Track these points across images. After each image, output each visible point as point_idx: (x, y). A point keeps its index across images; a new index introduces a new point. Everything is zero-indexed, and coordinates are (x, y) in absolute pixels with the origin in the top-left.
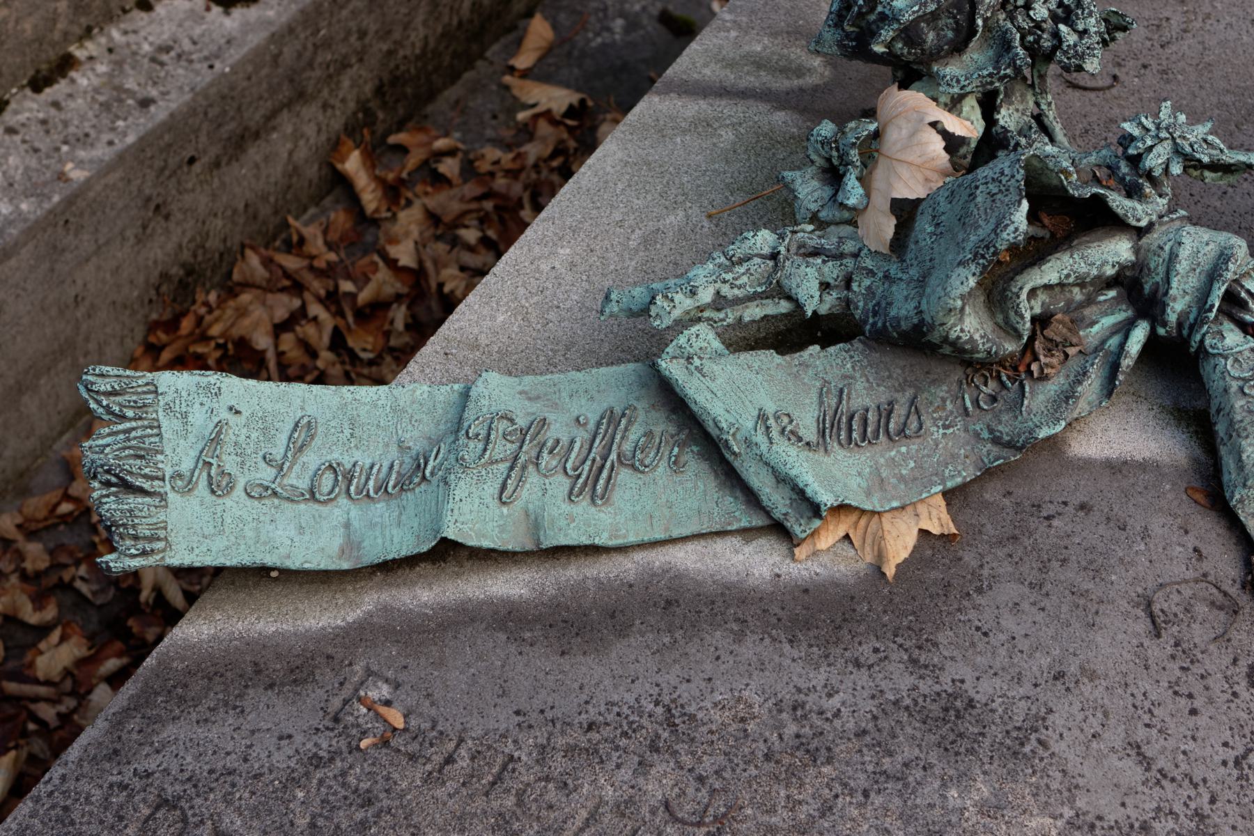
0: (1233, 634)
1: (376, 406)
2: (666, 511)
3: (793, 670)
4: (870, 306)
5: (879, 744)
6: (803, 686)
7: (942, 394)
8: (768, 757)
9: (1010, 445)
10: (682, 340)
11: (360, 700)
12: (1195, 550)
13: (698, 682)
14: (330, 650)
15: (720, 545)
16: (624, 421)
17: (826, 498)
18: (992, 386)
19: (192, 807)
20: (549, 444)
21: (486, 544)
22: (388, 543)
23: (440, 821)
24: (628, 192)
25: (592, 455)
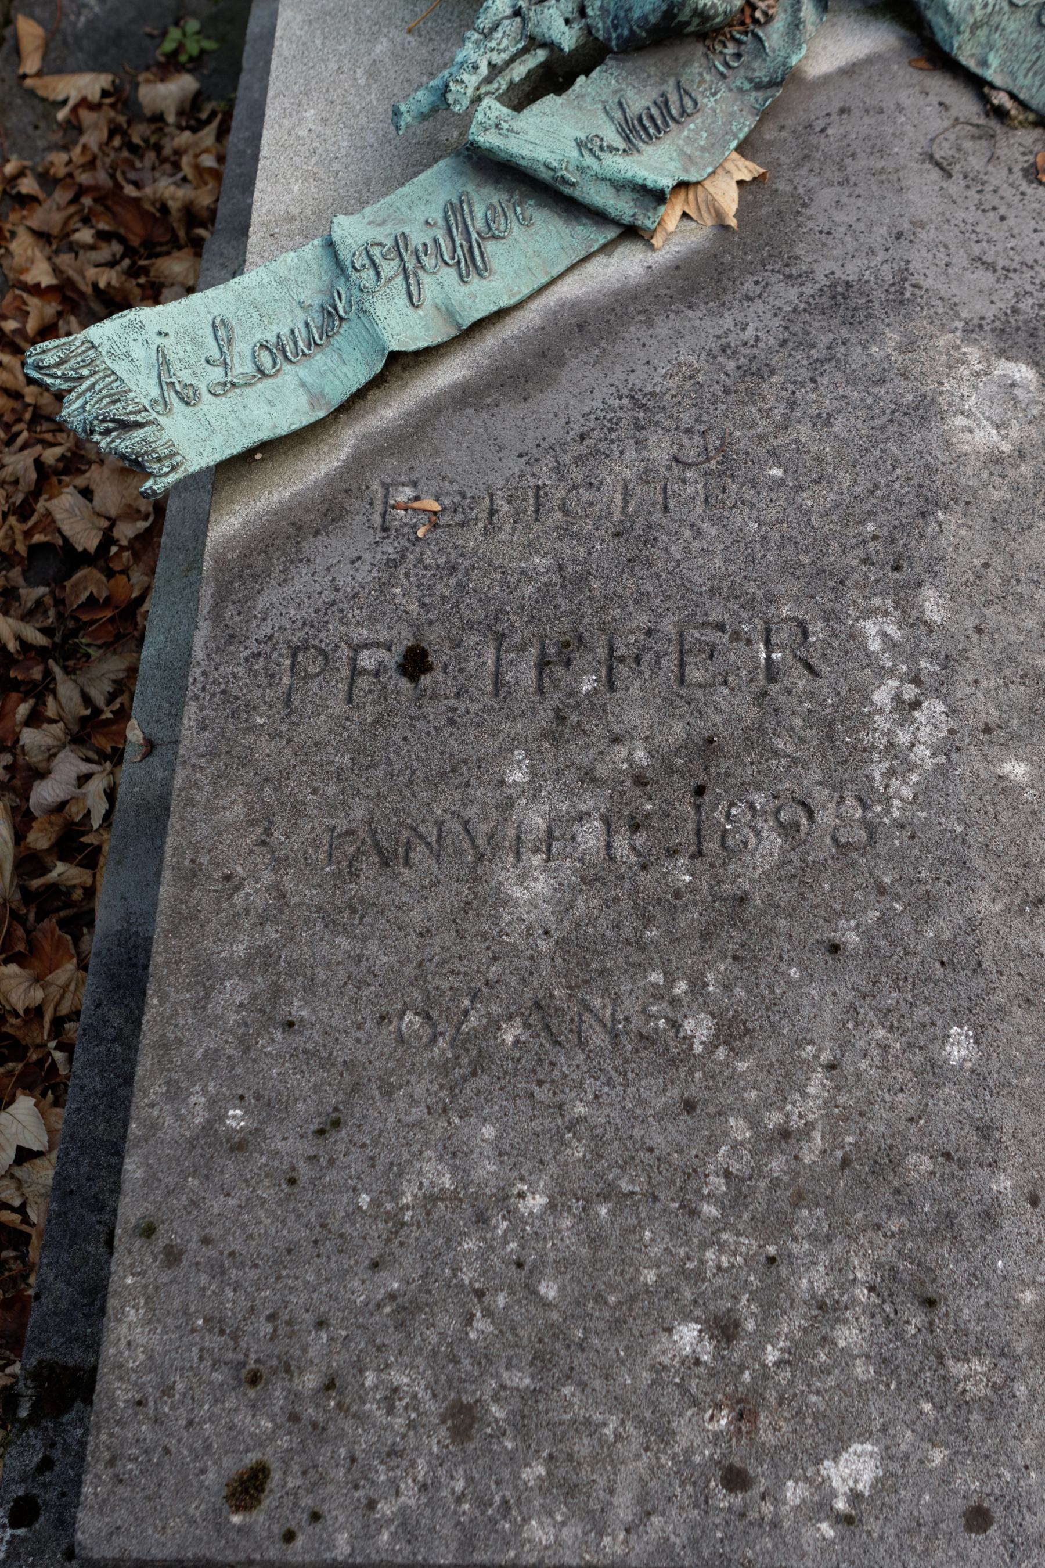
0: (999, 152)
1: (263, 286)
2: (538, 260)
3: (705, 326)
4: (609, 22)
5: (801, 344)
6: (720, 332)
7: (697, 70)
8: (727, 392)
9: (773, 84)
10: (480, 116)
11: (393, 507)
12: (941, 104)
13: (640, 369)
14: (345, 486)
15: (590, 267)
16: (465, 206)
17: (666, 182)
18: (731, 49)
19: (321, 641)
20: (421, 248)
21: (422, 344)
22: (345, 381)
23: (516, 554)
24: (327, 43)
25: (458, 243)
